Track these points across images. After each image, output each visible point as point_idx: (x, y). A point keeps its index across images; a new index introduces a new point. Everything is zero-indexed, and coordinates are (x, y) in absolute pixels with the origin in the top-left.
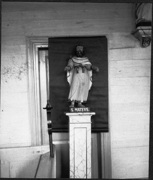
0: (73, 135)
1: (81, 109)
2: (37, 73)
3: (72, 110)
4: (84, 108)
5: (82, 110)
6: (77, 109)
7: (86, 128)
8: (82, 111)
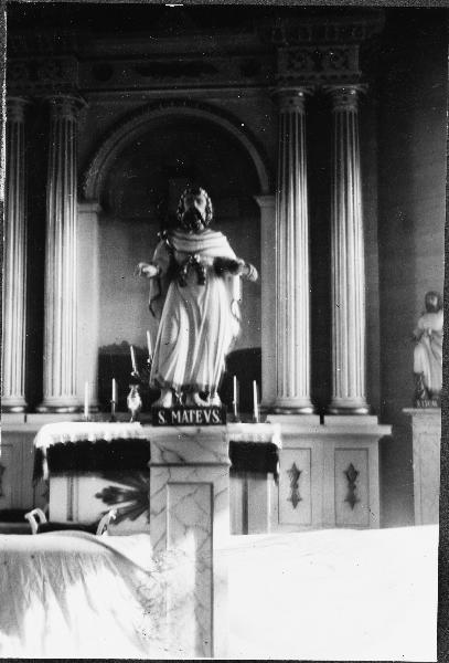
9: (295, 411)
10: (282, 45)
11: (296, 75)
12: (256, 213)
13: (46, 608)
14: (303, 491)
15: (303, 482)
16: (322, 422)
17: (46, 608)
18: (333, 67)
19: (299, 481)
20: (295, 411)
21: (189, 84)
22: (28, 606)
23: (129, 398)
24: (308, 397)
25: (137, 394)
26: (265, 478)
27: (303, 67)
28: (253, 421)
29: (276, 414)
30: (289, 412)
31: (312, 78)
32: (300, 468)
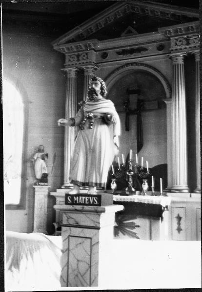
0: (66, 251)
1: (85, 199)
2: (86, 230)
3: (70, 200)
4: (90, 198)
5: (86, 200)
6: (77, 198)
7: (91, 238)
8: (86, 203)
9: (180, 191)
10: (172, 37)
11: (179, 48)
12: (165, 106)
13: (27, 259)
14: (183, 226)
15: (182, 222)
16: (191, 196)
17: (27, 259)
18: (83, 59)
19: (181, 222)
20: (180, 191)
21: (137, 57)
22: (22, 258)
23: (112, 184)
24: (186, 185)
25: (115, 183)
26: (159, 220)
27: (181, 44)
28: (159, 195)
29: (171, 192)
30: (177, 192)
31: (186, 48)
32: (181, 216)
